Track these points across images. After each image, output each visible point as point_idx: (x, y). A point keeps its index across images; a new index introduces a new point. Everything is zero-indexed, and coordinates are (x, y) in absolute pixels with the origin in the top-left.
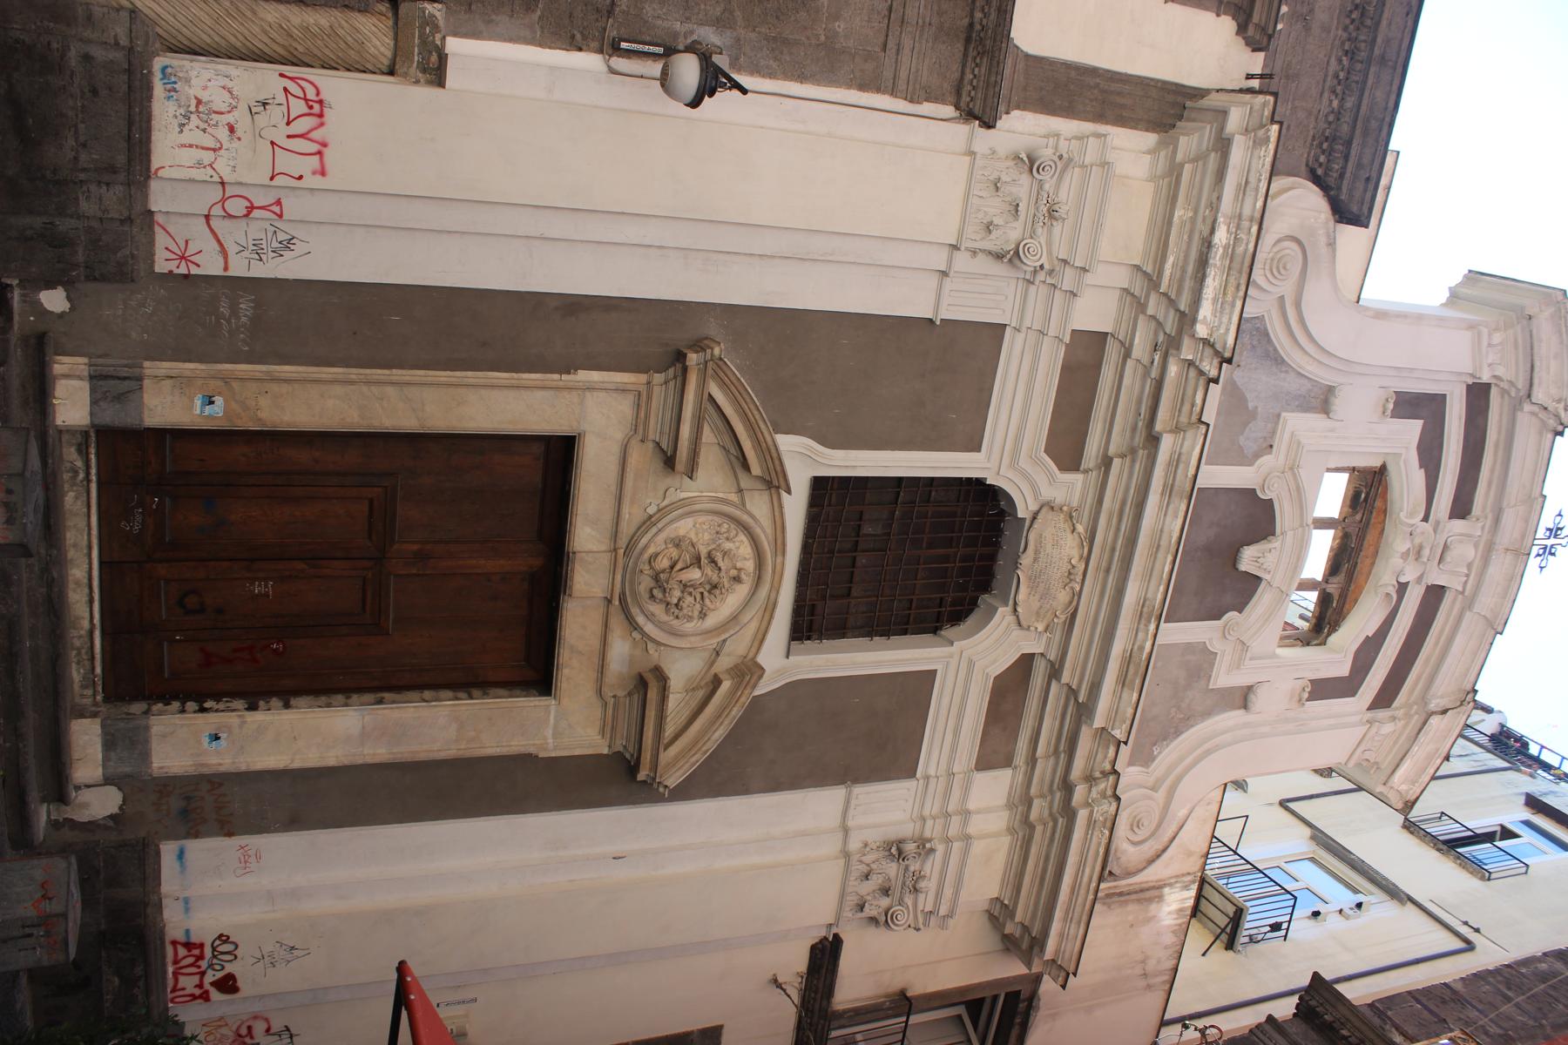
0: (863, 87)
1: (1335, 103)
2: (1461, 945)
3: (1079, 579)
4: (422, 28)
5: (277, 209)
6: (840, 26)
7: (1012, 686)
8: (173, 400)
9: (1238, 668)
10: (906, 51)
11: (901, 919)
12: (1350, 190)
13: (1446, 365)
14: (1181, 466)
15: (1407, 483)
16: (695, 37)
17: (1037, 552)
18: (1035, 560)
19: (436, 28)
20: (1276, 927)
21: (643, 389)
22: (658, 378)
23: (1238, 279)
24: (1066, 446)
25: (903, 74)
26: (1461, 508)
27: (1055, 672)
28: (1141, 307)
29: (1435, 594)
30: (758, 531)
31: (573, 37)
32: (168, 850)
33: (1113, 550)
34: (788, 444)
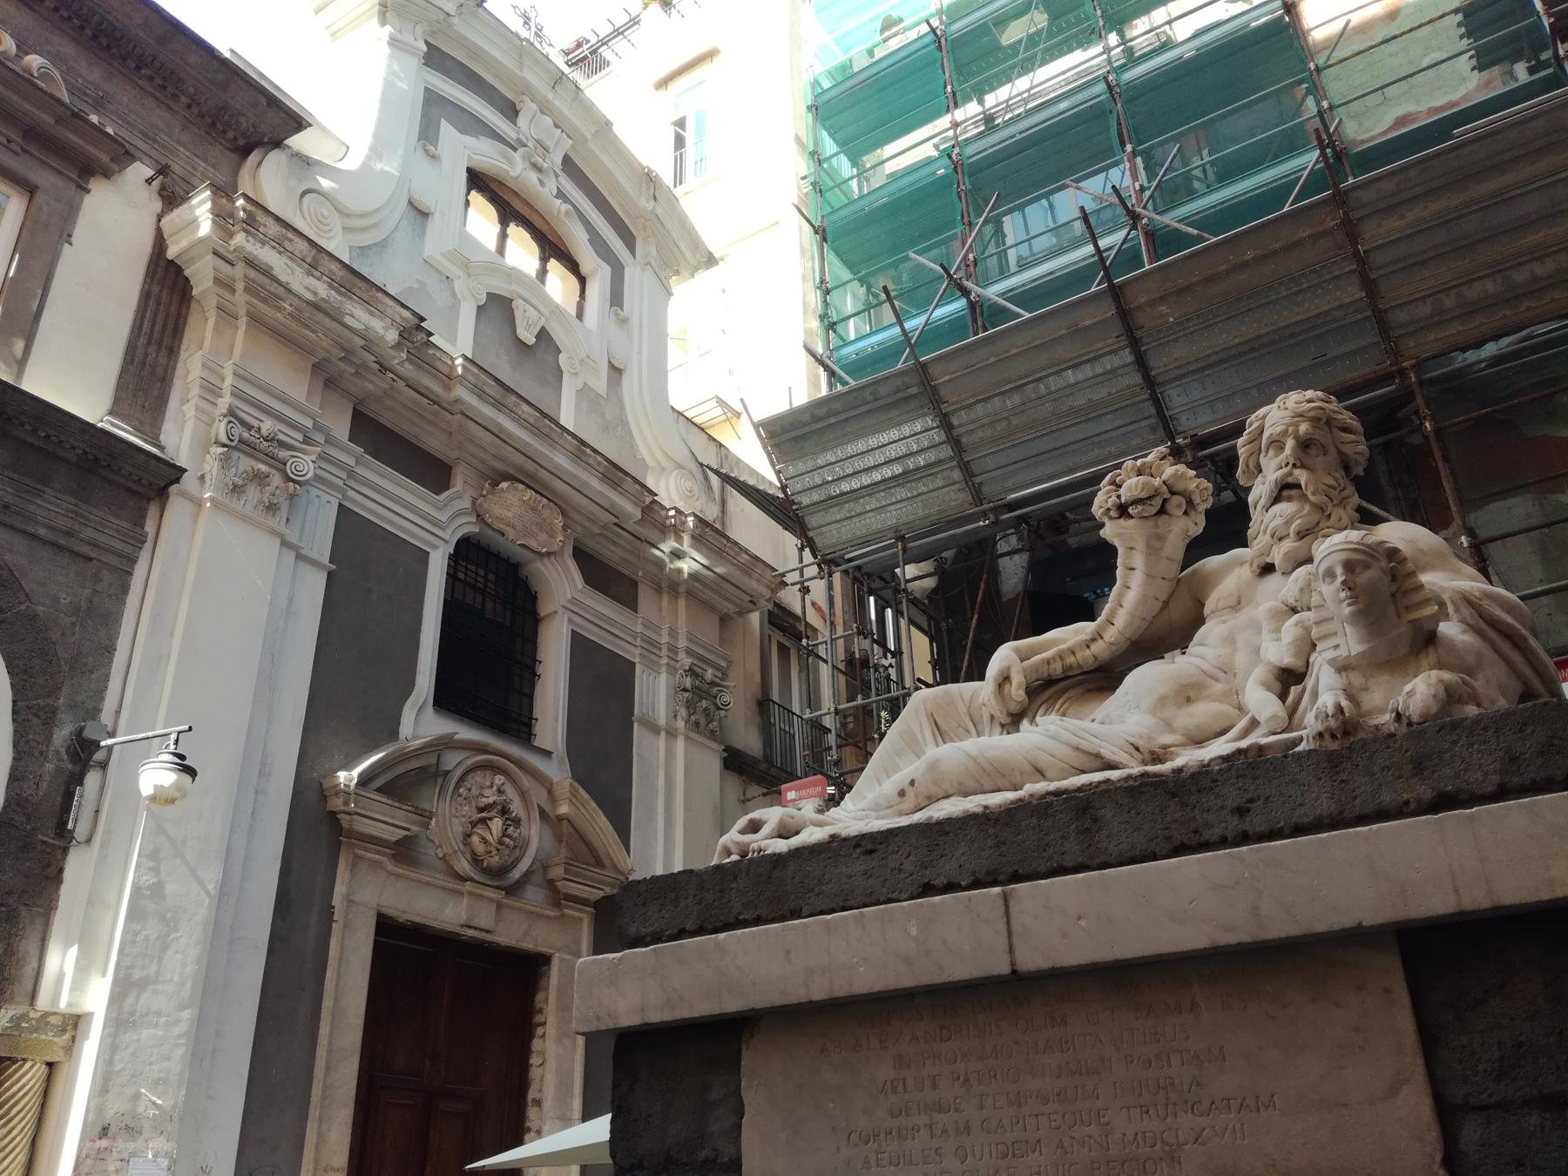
6: (65, 598)
10: (97, 536)
15: (487, 154)
16: (63, 750)
25: (119, 545)
29: (568, 163)
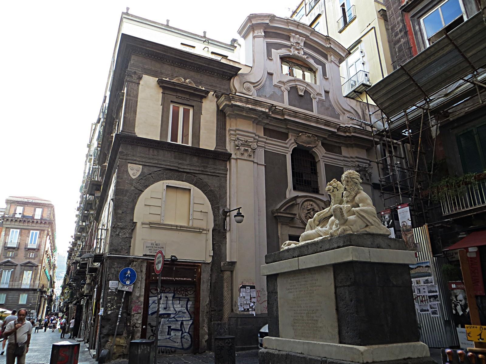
0: (226, 181)
1: (216, 74)
2: (373, 30)
3: (309, 135)
4: (225, 266)
7: (328, 147)
9: (321, 95)
11: (370, 171)
12: (233, 72)
13: (262, 43)
18: (305, 143)
19: (225, 263)
20: (366, 75)
21: (281, 223)
22: (279, 220)
23: (258, 103)
24: (284, 136)
26: (288, 38)
27: (325, 139)
28: (260, 121)
30: (303, 200)
33: (304, 127)
34: (288, 196)
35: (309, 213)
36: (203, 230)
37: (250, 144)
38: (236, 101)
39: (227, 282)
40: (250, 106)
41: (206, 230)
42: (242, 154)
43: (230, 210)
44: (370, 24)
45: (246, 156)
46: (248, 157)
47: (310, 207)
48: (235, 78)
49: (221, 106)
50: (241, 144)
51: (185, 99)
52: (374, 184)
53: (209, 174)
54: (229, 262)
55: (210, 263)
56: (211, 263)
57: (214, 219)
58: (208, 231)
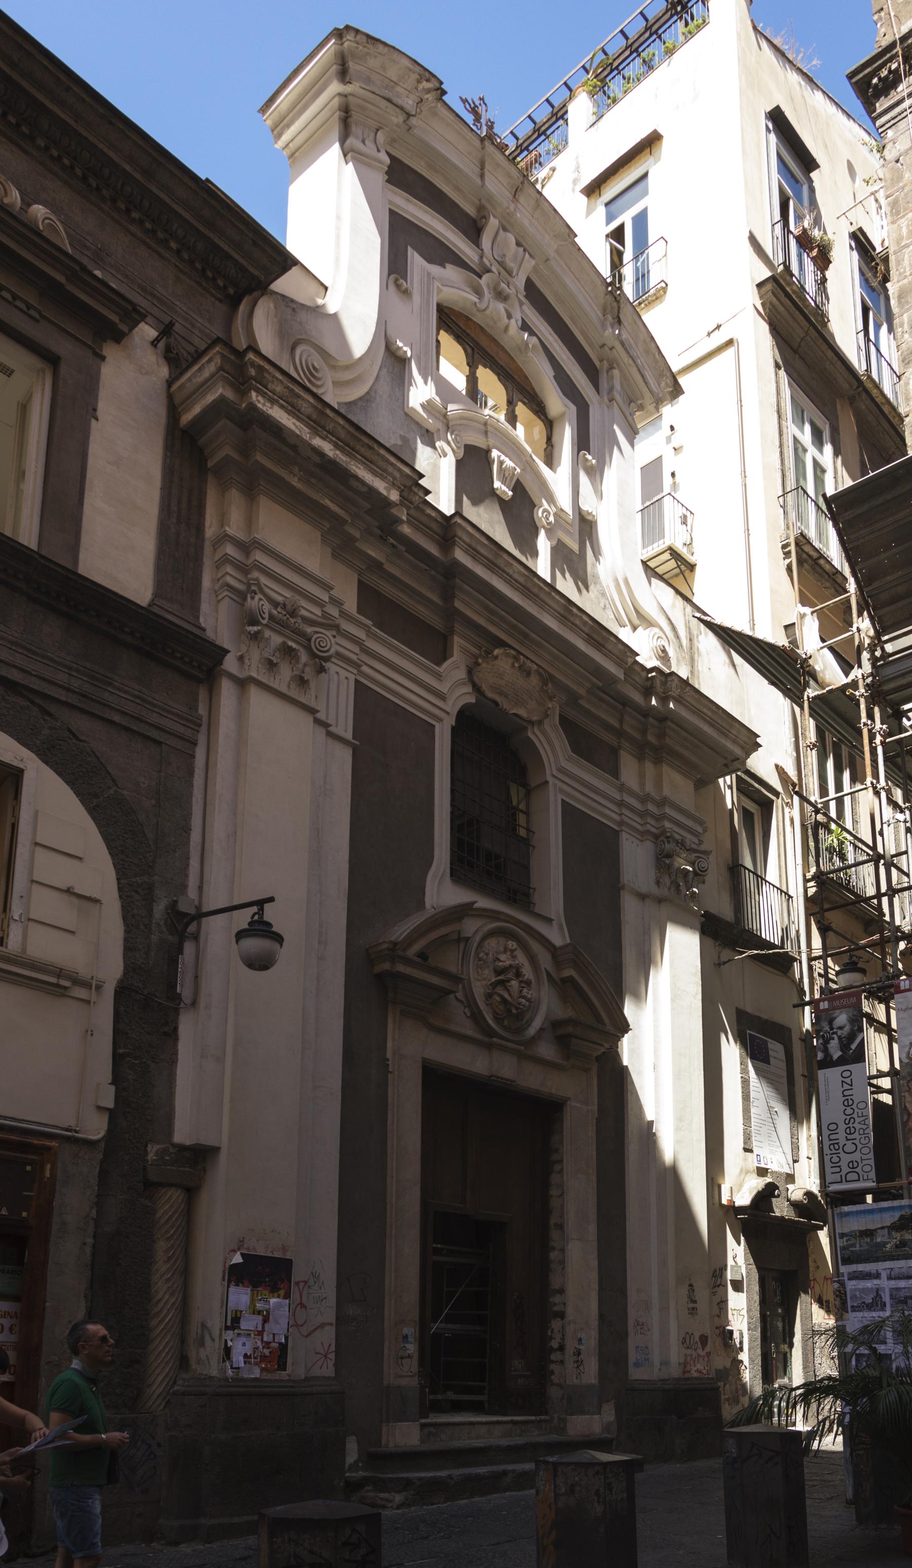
0: (191, 773)
2: (731, 351)
5: (302, 1285)
8: (403, 1368)
14: (479, 548)
17: (501, 693)
18: (506, 696)
24: (437, 648)
26: (473, 229)
29: (532, 292)
31: (165, 1034)
32: (636, 1374)
35: (502, 983)
36: (78, 982)
37: (309, 630)
38: (272, 401)
39: (168, 1239)
40: (327, 448)
41: (86, 985)
42: (271, 665)
43: (199, 908)
44: (719, 327)
45: (283, 679)
46: (293, 685)
47: (505, 960)
48: (261, 302)
49: (187, 410)
50: (271, 617)
51: (18, 303)
52: (707, 915)
53: (117, 718)
54: (182, 1148)
55: (99, 1141)
56: (103, 1145)
57: (126, 940)
58: (99, 988)
